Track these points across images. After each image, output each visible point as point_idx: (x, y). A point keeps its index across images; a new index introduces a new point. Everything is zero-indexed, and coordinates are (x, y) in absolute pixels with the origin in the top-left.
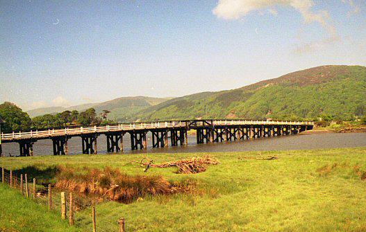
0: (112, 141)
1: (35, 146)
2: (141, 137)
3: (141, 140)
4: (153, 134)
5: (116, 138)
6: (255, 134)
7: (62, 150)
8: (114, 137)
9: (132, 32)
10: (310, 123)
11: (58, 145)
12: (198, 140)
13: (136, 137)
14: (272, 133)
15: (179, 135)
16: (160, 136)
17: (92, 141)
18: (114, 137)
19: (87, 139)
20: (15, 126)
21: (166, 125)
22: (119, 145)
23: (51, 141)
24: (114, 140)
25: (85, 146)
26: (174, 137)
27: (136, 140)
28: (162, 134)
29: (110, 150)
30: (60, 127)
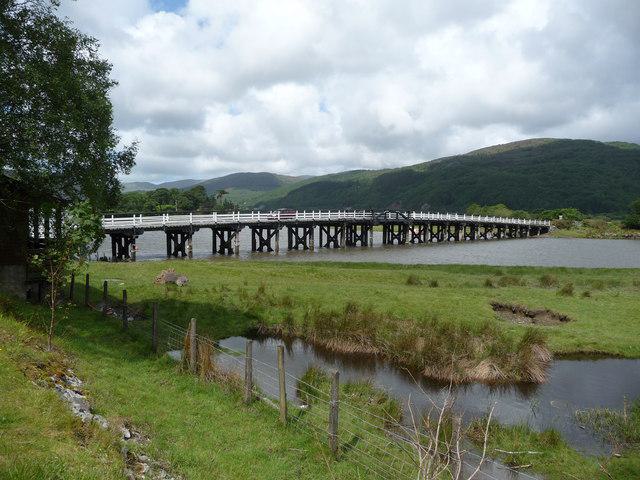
0: (261, 239)
1: (196, 235)
2: (305, 233)
3: (305, 238)
4: (290, 233)
5: (269, 233)
6: (330, 239)
7: (182, 249)
8: (226, 233)
9: (625, 446)
10: (545, 223)
11: (120, 244)
12: (384, 242)
13: (296, 233)
14: (461, 235)
15: (359, 233)
17: (127, 244)
18: (226, 233)
19: (223, 233)
20: (219, 202)
21: (276, 216)
22: (233, 245)
23: (163, 235)
24: (265, 237)
25: (173, 246)
26: (521, 233)
27: (297, 237)
29: (117, 259)
30: (186, 211)
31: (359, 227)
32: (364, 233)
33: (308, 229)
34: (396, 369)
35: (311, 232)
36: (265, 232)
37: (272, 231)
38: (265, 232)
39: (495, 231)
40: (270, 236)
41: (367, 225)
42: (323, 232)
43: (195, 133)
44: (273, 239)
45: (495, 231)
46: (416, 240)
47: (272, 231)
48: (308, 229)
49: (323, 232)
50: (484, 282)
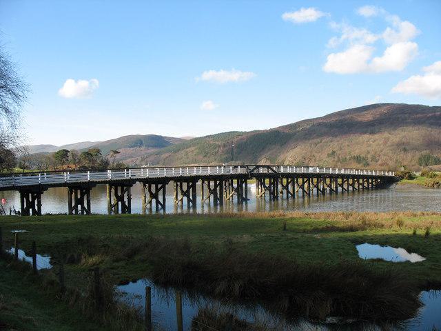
5: (157, 187)
11: (28, 200)
16: (212, 188)
28: (215, 183)
31: (235, 181)
32: (240, 185)
33: (191, 184)
34: (372, 323)
35: (194, 187)
36: (153, 187)
37: (160, 186)
38: (153, 187)
39: (351, 181)
40: (157, 190)
41: (243, 179)
42: (292, 192)
43: (421, 310)
44: (161, 192)
45: (328, 180)
46: (340, 189)
47: (160, 186)
48: (218, 182)
49: (292, 192)
50: (403, 228)
